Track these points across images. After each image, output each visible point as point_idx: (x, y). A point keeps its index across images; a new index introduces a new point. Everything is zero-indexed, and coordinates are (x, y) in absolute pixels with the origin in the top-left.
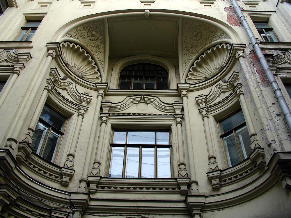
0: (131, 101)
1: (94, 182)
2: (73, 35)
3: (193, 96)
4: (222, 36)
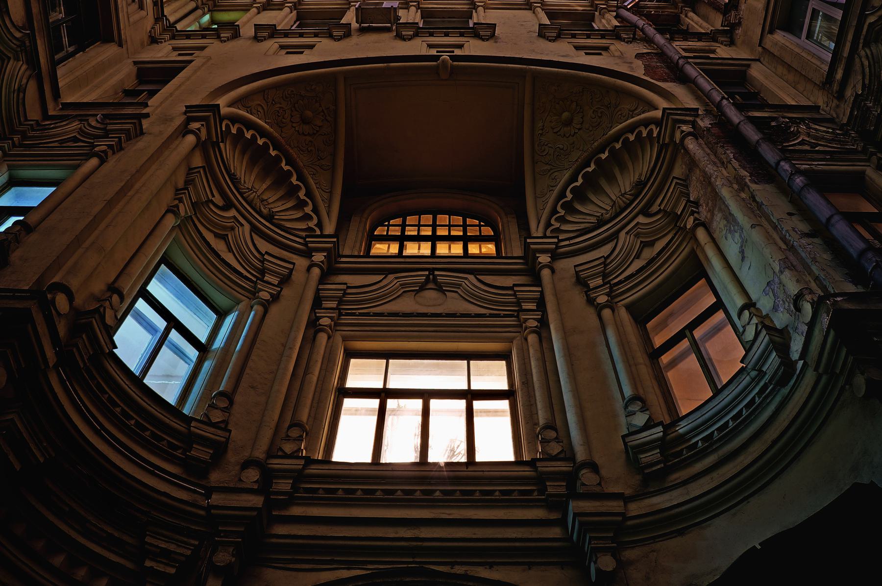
0: (401, 285)
1: (284, 474)
2: (253, 111)
3: (567, 265)
4: (635, 109)
